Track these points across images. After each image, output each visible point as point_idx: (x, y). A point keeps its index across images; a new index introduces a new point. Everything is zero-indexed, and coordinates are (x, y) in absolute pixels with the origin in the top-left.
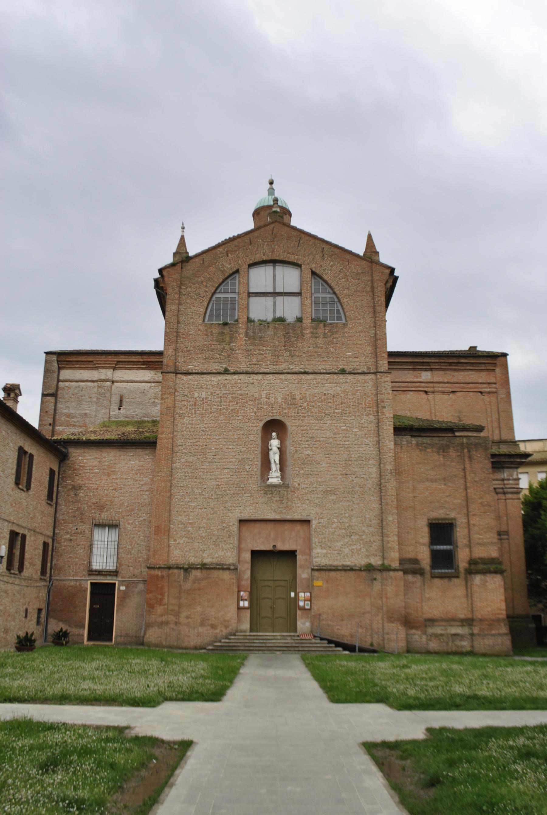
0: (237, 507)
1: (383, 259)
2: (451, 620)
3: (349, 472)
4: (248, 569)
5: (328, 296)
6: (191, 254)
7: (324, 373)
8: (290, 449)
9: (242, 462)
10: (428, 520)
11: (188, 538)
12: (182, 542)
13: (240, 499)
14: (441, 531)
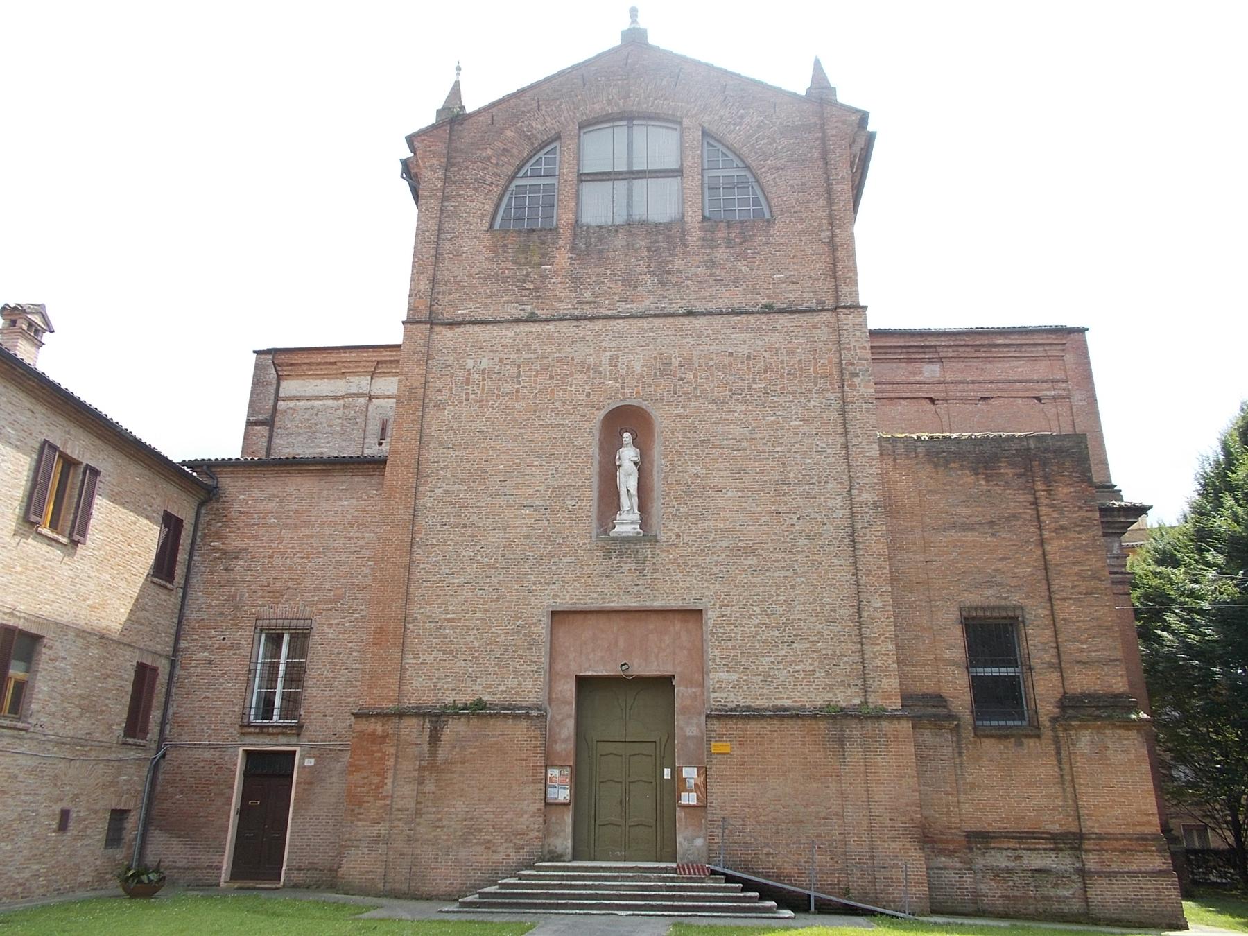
0: (548, 584)
1: (843, 98)
2: (1027, 838)
3: (783, 509)
4: (569, 716)
5: (736, 173)
6: (469, 110)
7: (728, 314)
8: (659, 463)
9: (559, 491)
10: (961, 609)
11: (444, 652)
12: (430, 659)
13: (554, 568)
14: (991, 637)
